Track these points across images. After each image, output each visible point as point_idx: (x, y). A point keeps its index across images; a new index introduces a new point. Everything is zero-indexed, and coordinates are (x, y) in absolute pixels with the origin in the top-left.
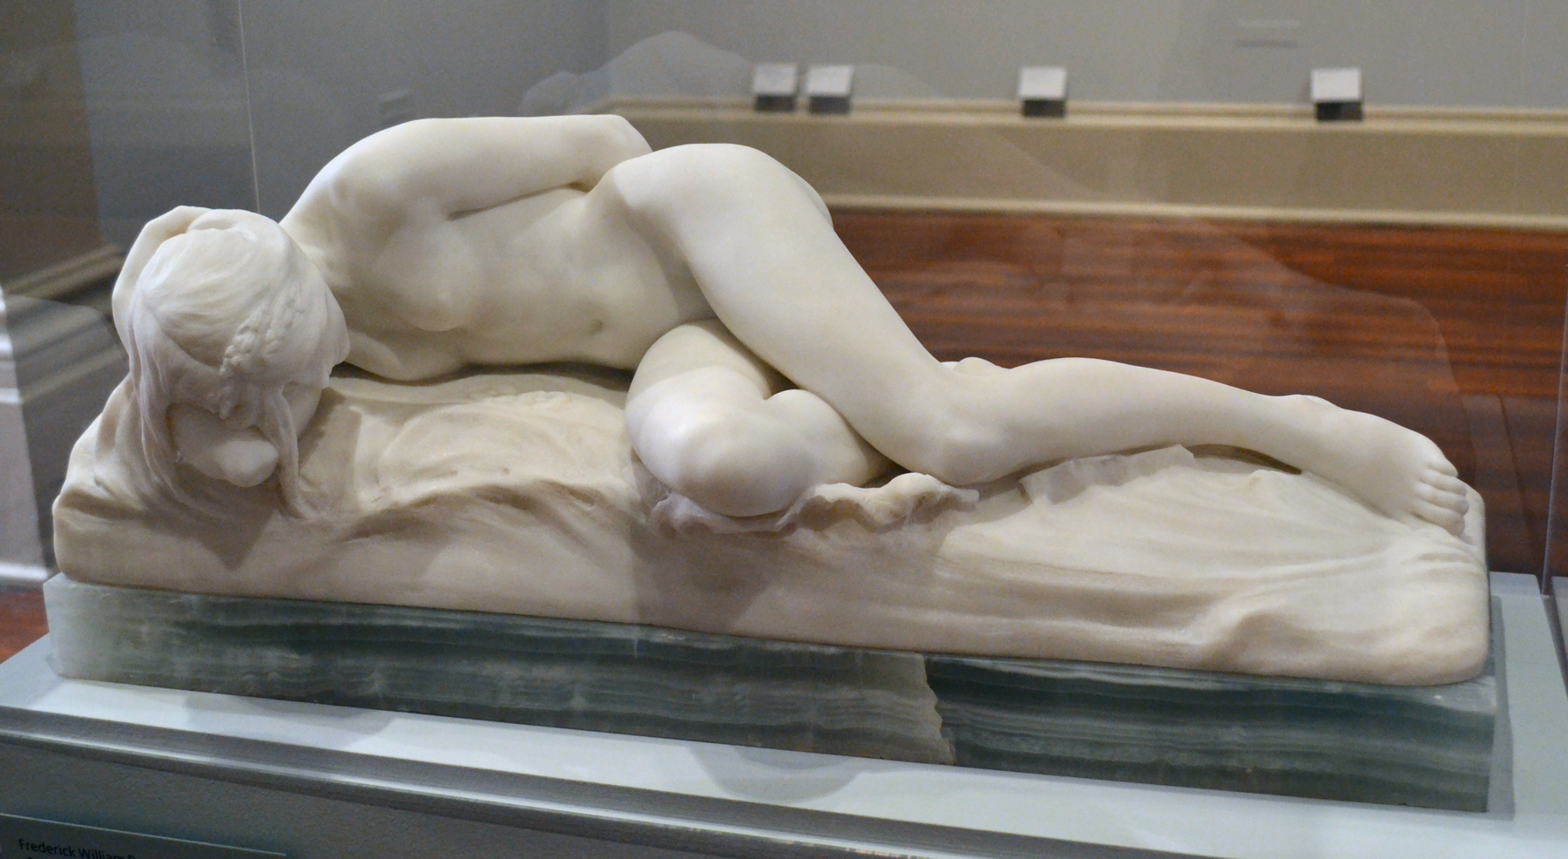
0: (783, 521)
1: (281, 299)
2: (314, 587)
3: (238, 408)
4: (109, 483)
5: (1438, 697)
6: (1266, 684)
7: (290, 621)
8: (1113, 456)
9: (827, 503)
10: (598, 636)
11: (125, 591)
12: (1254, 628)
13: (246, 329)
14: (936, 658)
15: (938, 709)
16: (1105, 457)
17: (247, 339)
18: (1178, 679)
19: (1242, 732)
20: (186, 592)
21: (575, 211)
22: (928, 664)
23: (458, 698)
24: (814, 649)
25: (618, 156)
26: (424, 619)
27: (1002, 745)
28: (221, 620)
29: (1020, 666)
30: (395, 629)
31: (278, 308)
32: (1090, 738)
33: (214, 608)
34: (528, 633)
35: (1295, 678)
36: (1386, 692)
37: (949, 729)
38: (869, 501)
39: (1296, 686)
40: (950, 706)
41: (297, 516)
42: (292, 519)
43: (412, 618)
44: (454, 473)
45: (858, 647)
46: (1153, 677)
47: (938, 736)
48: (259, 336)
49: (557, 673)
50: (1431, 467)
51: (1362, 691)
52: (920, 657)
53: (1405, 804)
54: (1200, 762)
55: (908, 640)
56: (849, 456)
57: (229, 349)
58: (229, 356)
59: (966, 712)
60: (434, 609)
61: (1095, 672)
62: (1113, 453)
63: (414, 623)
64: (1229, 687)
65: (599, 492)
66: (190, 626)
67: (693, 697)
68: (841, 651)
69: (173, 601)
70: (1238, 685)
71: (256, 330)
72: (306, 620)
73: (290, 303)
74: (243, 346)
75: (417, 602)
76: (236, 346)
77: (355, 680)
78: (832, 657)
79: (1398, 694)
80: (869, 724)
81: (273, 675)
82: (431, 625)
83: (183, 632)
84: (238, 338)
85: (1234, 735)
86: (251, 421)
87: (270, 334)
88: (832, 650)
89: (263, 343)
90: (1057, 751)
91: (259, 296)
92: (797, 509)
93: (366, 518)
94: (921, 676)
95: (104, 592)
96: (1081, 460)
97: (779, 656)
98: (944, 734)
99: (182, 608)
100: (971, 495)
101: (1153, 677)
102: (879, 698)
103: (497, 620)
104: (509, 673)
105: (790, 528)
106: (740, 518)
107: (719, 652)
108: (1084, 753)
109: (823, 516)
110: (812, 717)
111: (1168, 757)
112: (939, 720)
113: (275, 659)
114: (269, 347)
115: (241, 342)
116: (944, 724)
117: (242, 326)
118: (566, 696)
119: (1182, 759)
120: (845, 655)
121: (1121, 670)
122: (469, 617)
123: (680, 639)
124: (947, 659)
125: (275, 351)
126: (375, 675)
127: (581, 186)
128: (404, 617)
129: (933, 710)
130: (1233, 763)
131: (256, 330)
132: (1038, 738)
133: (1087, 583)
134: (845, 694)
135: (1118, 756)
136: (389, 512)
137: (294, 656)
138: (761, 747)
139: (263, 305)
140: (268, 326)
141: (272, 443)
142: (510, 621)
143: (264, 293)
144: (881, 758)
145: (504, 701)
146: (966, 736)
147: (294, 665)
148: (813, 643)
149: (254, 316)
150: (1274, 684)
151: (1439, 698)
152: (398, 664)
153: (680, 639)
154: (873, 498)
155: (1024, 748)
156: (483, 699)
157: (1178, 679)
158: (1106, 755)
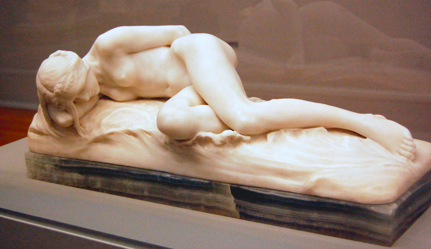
0: (190, 142)
1: (71, 75)
2: (84, 156)
3: (60, 104)
4: (38, 126)
5: (372, 208)
6: (323, 200)
7: (78, 166)
8: (299, 129)
9: (202, 137)
10: (148, 174)
11: (42, 155)
12: (320, 182)
13: (60, 82)
14: (233, 186)
15: (235, 202)
16: (295, 129)
17: (59, 85)
18: (298, 196)
19: (317, 215)
20: (56, 156)
21: (164, 52)
22: (231, 187)
23: (118, 190)
24: (202, 181)
25: (178, 36)
26: (109, 167)
27: (253, 214)
28: (63, 165)
29: (255, 189)
30: (101, 169)
31: (69, 78)
32: (276, 213)
33: (61, 161)
34: (133, 172)
35: (332, 199)
36: (357, 205)
37: (238, 208)
38: (215, 137)
39: (331, 201)
40: (237, 201)
41: (80, 136)
42: (79, 137)
43: (106, 166)
44: (120, 126)
45: (214, 181)
46: (291, 195)
47: (235, 210)
48: (63, 84)
49: (140, 184)
50: (405, 138)
51: (351, 204)
52: (229, 185)
53: (365, 242)
54: (305, 223)
55: (225, 179)
56: (217, 125)
57: (55, 88)
58: (55, 90)
59: (242, 203)
60: (113, 164)
61: (276, 193)
62: (298, 128)
63: (107, 168)
64: (312, 200)
65: (152, 133)
66: (56, 166)
67: (173, 194)
68: (209, 182)
69: (52, 159)
70: (315, 200)
71: (62, 83)
72: (82, 166)
73: (73, 77)
74: (59, 87)
75: (108, 162)
76: (57, 87)
77: (94, 183)
78: (206, 183)
79: (362, 206)
80: (217, 205)
81: (76, 181)
82: (110, 168)
83: (55, 167)
84: (57, 85)
85: (314, 215)
86: (64, 108)
87: (66, 84)
88: (206, 182)
89: (64, 87)
90: (267, 217)
91: (64, 74)
92: (194, 138)
93: (96, 138)
94: (229, 191)
95: (38, 155)
96: (286, 129)
97: (193, 182)
98: (237, 209)
99: (54, 161)
100: (248, 138)
101: (291, 195)
102: (220, 197)
103: (126, 168)
104: (128, 183)
105: (194, 144)
106: (178, 140)
107: (178, 180)
108: (275, 218)
109: (206, 141)
110: (203, 202)
111: (297, 221)
112: (235, 205)
113: (76, 176)
114: (65, 88)
115: (58, 86)
116: (237, 206)
117: (59, 82)
118: (143, 191)
119: (301, 222)
120: (210, 183)
121: (284, 193)
122: (120, 167)
123: (169, 176)
124: (236, 186)
125: (67, 89)
126: (98, 182)
127: (169, 46)
128: (104, 166)
129: (233, 201)
130: (315, 224)
131: (62, 83)
132: (261, 212)
133: (275, 166)
134: (210, 195)
135: (283, 220)
136: (102, 136)
137: (80, 175)
138: (191, 209)
139: (65, 76)
140: (66, 82)
141: (71, 115)
142: (128, 168)
143: (66, 73)
144: (221, 215)
145: (129, 191)
146: (243, 210)
147: (80, 178)
148: (201, 179)
149: (62, 80)
150: (337, 202)
151: (373, 208)
152: (78, 175)
153: (169, 176)
154: (217, 137)
155: (258, 215)
156: (123, 191)
157: (298, 196)
158: (280, 219)
